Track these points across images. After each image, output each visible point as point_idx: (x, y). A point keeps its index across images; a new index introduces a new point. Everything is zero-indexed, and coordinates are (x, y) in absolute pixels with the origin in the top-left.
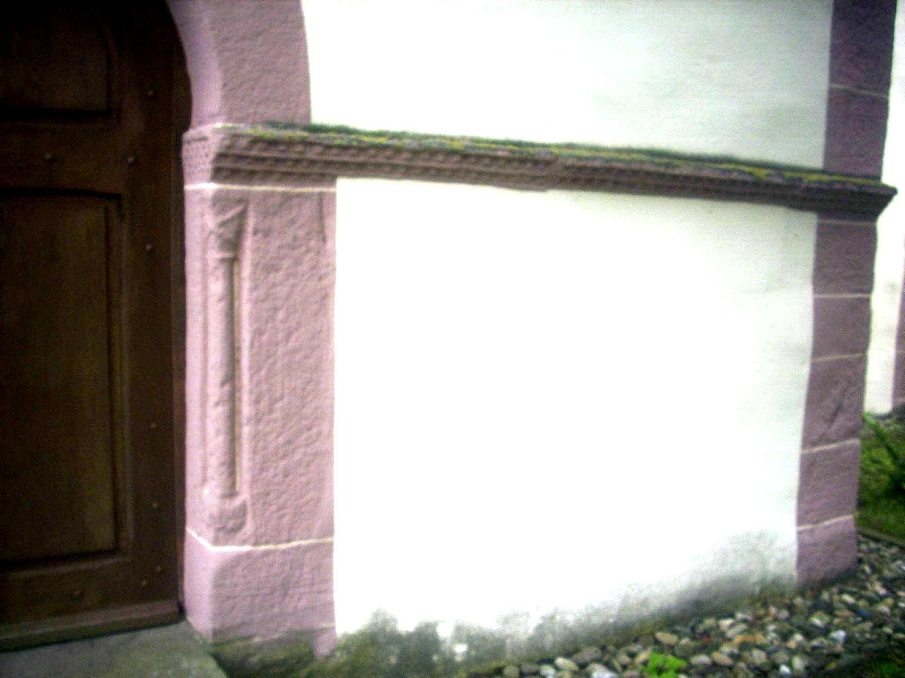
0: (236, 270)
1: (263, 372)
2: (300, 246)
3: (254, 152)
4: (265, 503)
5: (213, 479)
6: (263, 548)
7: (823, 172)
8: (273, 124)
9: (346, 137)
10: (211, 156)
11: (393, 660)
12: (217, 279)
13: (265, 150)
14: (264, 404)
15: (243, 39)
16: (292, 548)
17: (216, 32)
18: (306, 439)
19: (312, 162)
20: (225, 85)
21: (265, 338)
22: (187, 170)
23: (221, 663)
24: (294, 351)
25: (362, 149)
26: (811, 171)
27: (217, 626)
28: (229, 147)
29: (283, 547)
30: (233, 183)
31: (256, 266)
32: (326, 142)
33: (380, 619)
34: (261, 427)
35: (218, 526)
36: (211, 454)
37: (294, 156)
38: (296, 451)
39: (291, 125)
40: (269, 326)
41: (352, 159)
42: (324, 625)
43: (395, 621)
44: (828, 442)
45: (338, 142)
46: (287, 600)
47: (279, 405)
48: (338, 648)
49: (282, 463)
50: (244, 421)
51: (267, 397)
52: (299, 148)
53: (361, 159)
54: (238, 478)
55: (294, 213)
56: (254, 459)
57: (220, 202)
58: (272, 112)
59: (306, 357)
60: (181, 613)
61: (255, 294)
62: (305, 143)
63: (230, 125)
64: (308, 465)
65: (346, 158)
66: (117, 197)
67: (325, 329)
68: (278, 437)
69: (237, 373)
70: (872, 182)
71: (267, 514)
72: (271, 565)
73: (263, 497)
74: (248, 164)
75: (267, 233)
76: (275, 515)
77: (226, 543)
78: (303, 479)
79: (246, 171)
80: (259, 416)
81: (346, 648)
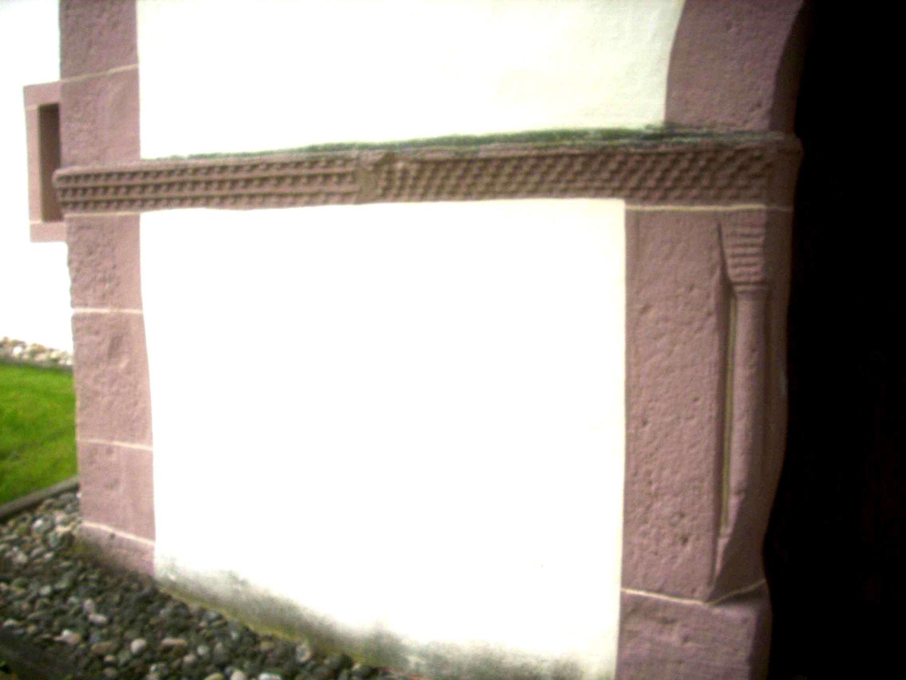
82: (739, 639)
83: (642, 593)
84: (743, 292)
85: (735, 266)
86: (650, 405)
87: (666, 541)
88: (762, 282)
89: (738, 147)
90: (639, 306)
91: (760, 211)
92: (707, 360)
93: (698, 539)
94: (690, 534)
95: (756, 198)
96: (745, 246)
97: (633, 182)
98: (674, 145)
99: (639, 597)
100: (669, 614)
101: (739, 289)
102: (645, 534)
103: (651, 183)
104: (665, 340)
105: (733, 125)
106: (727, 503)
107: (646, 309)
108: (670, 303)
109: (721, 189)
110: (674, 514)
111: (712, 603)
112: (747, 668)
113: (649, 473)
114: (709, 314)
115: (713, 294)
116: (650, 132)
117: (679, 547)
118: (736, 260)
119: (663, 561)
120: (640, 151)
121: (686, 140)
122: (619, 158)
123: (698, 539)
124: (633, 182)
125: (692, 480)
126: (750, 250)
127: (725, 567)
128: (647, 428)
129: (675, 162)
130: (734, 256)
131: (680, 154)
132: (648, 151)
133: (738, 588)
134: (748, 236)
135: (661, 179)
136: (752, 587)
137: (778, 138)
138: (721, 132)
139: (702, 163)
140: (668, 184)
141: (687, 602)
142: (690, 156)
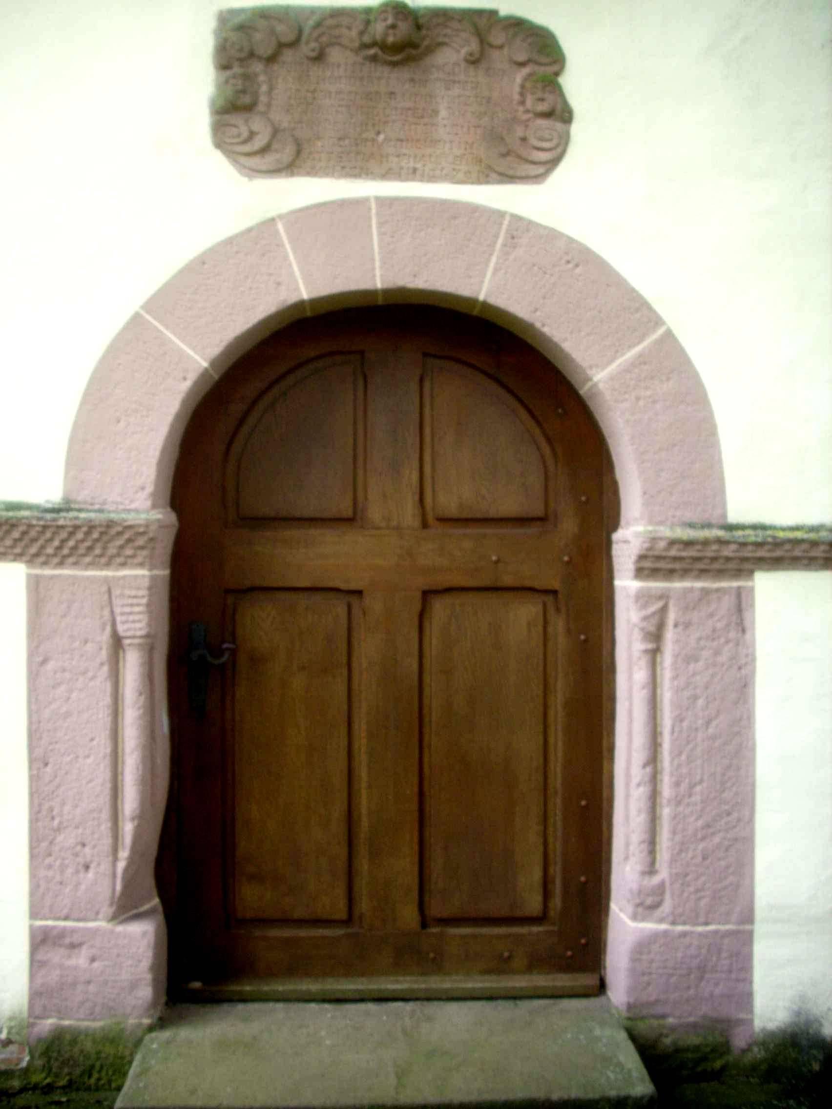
0: (658, 659)
1: (683, 757)
2: (719, 637)
3: (673, 552)
4: (682, 884)
5: (634, 855)
6: (680, 928)
8: (691, 526)
9: (760, 533)
10: (634, 558)
11: (816, 1067)
12: (640, 669)
13: (684, 550)
14: (684, 786)
15: (660, 449)
16: (710, 932)
17: (635, 447)
18: (726, 823)
19: (728, 559)
20: (645, 493)
21: (685, 724)
23: (633, 1037)
24: (714, 738)
25: (778, 544)
27: (632, 1000)
28: (650, 549)
29: (700, 929)
30: (656, 580)
31: (676, 656)
32: (741, 540)
33: (803, 1019)
34: (681, 809)
35: (638, 901)
36: (633, 832)
37: (709, 554)
39: (708, 526)
40: (690, 713)
41: (768, 555)
42: (742, 1016)
43: (821, 1025)
45: (752, 539)
46: (703, 984)
47: (698, 788)
48: (756, 1043)
49: (701, 846)
50: (665, 801)
51: (687, 780)
52: (715, 547)
53: (778, 553)
54: (658, 857)
55: (713, 606)
56: (672, 840)
57: (643, 599)
58: (689, 515)
59: (725, 744)
60: (601, 987)
61: (676, 683)
62: (720, 541)
63: (650, 528)
64: (727, 850)
65: (761, 553)
66: (555, 592)
67: (745, 717)
68: (697, 819)
69: (659, 756)
71: (686, 894)
72: (689, 946)
73: (681, 878)
74: (668, 563)
75: (687, 625)
76: (693, 897)
77: (643, 920)
78: (723, 863)
79: (666, 570)
80: (678, 799)
81: (763, 1044)
82: (141, 950)
83: (50, 923)
84: (129, 645)
85: (124, 623)
86: (51, 747)
87: (70, 871)
88: (147, 636)
89: (126, 524)
90: (39, 659)
91: (143, 576)
92: (101, 704)
93: (99, 864)
94: (91, 862)
95: (141, 565)
96: (132, 605)
97: (33, 550)
98: (71, 519)
99: (47, 927)
100: (76, 939)
101: (127, 642)
102: (50, 867)
103: (50, 550)
104: (63, 688)
105: (122, 504)
106: (123, 829)
107: (44, 662)
108: (67, 656)
109: (112, 557)
110: (77, 844)
111: (116, 921)
112: (149, 977)
113: (51, 809)
114: (102, 664)
115: (105, 647)
116: (50, 506)
117: (82, 875)
118: (124, 618)
119: (68, 890)
120: (42, 523)
121: (83, 515)
122: (22, 528)
123: (99, 864)
124: (33, 550)
125: (92, 811)
126: (137, 609)
127: (124, 893)
128: (48, 769)
129: (72, 534)
130: (122, 614)
131: (77, 528)
132: (49, 523)
133: (136, 908)
134: (135, 597)
135: (59, 548)
136: (146, 907)
137: (160, 516)
138: (111, 509)
139: (95, 535)
140: (66, 551)
141: (91, 925)
142: (85, 529)
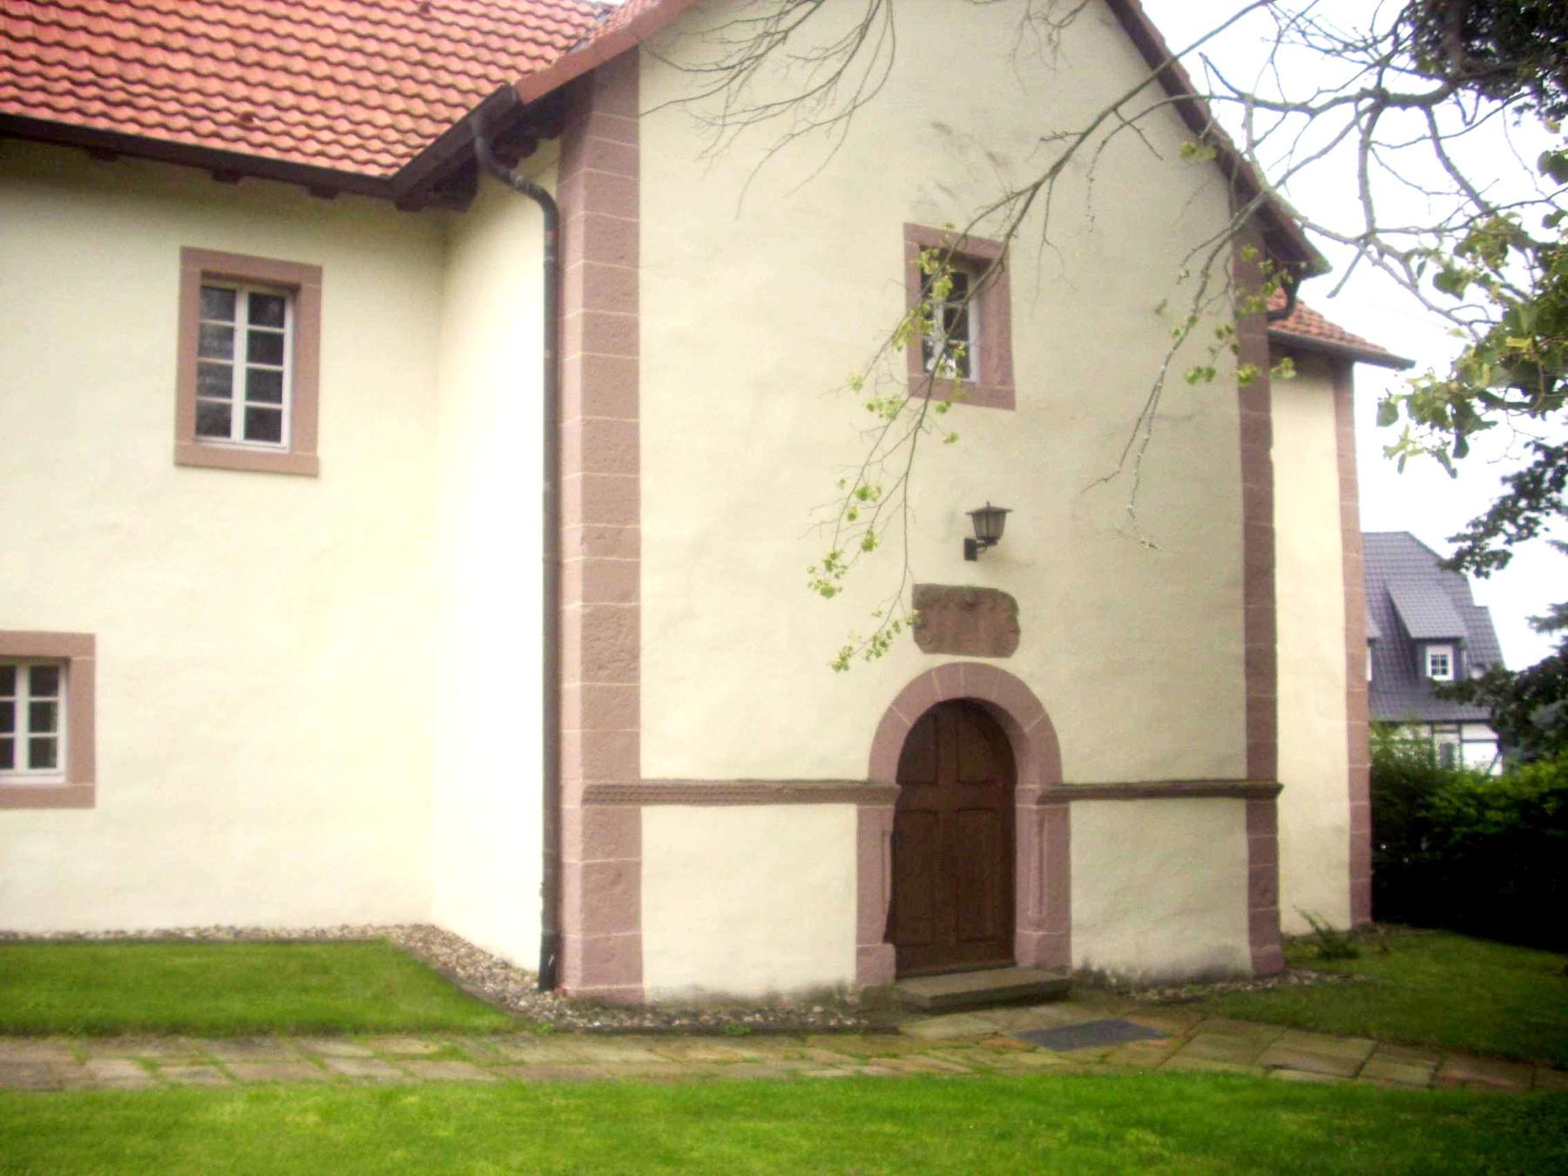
7: (1247, 780)
22: (1017, 799)
26: (1242, 780)
38: (182, 1040)
44: (1263, 906)
70: (1269, 783)
